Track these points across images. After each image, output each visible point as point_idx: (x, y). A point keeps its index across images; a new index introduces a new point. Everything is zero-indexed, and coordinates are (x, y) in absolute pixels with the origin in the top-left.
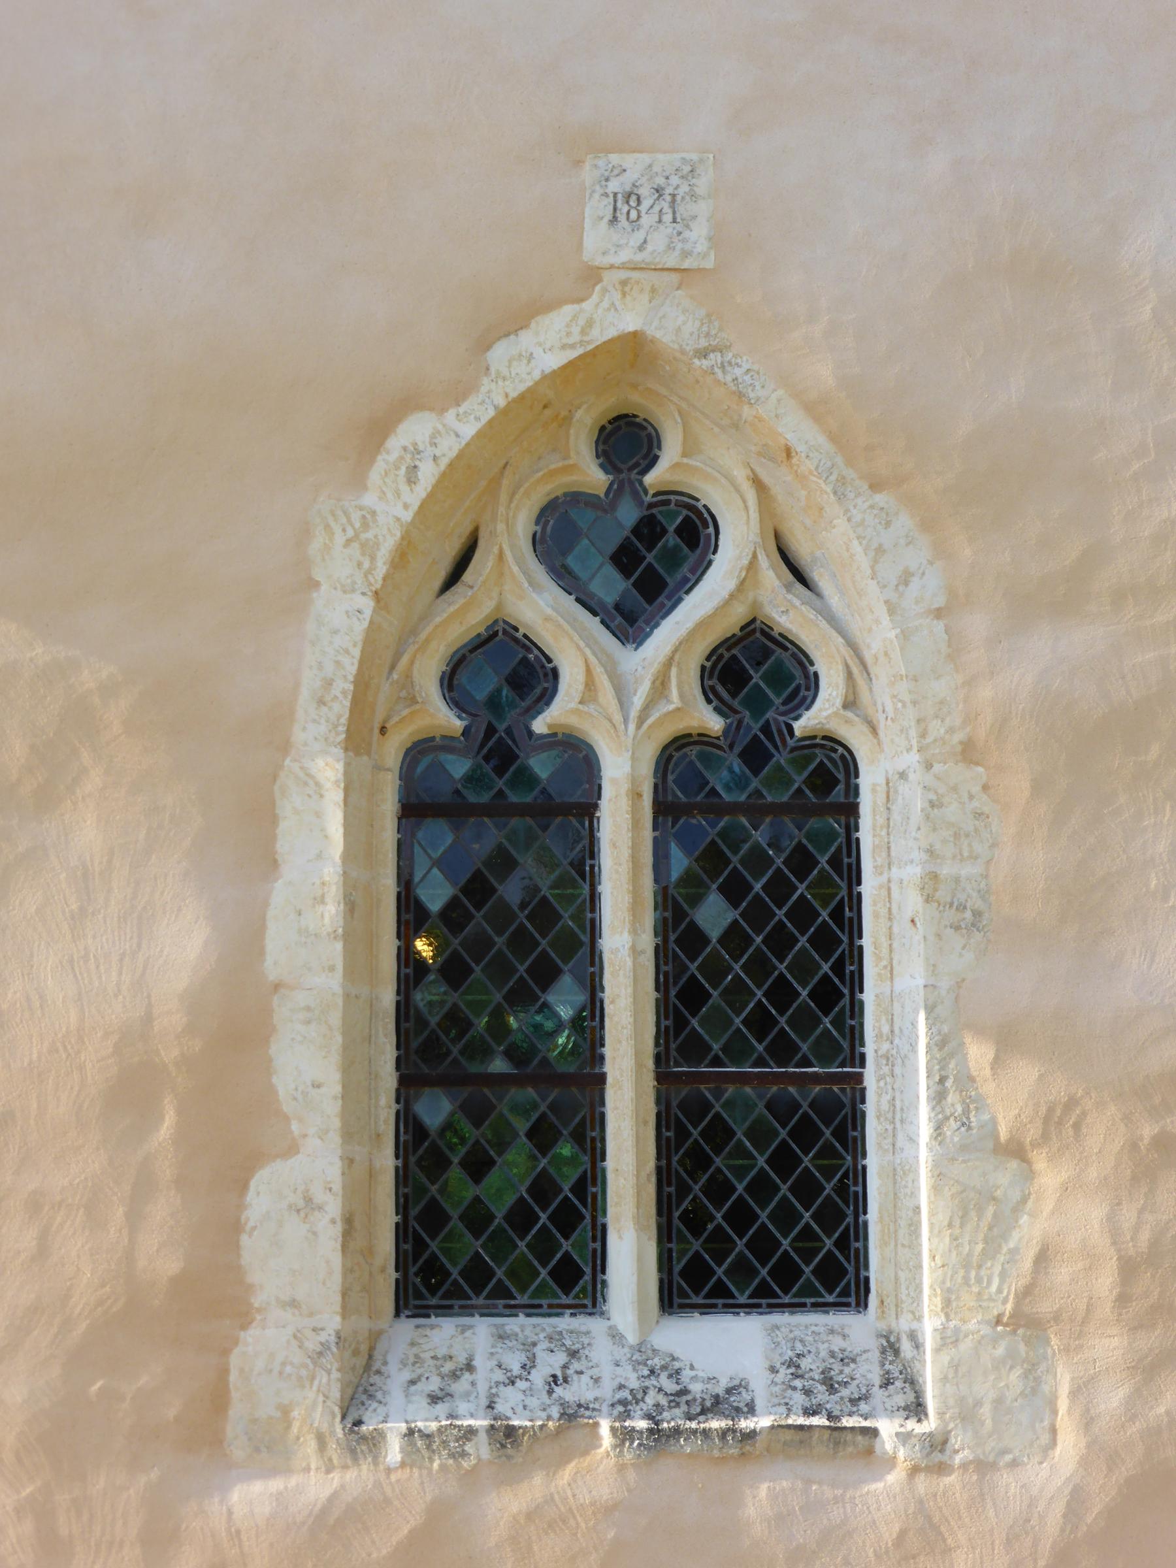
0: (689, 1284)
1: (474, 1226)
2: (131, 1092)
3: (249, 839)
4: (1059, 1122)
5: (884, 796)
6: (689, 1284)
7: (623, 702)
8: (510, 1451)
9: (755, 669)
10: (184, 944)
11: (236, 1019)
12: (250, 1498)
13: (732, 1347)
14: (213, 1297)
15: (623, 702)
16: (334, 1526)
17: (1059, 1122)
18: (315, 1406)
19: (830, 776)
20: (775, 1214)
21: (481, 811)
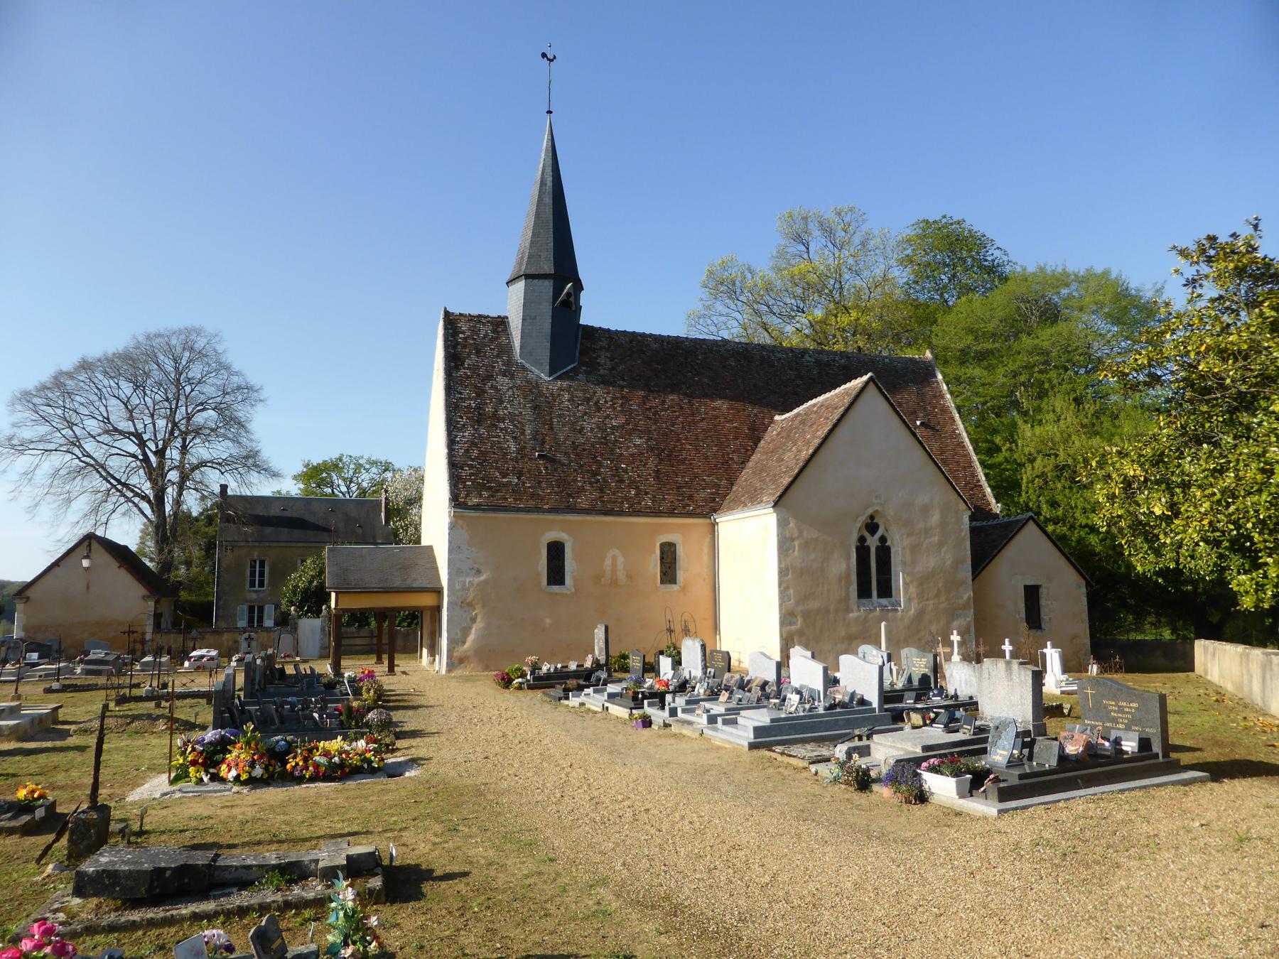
0: (879, 596)
1: (864, 592)
2: (840, 580)
3: (848, 558)
4: (912, 582)
5: (11, 771)
6: (879, 596)
7: (873, 542)
8: (263, 395)
9: (883, 539)
10: (844, 566)
11: (848, 573)
12: (851, 615)
13: (884, 601)
14: (847, 598)
15: (873, 542)
16: (858, 618)
17: (912, 582)
18: (855, 607)
19: (888, 549)
20: (886, 590)
21: (862, 551)
